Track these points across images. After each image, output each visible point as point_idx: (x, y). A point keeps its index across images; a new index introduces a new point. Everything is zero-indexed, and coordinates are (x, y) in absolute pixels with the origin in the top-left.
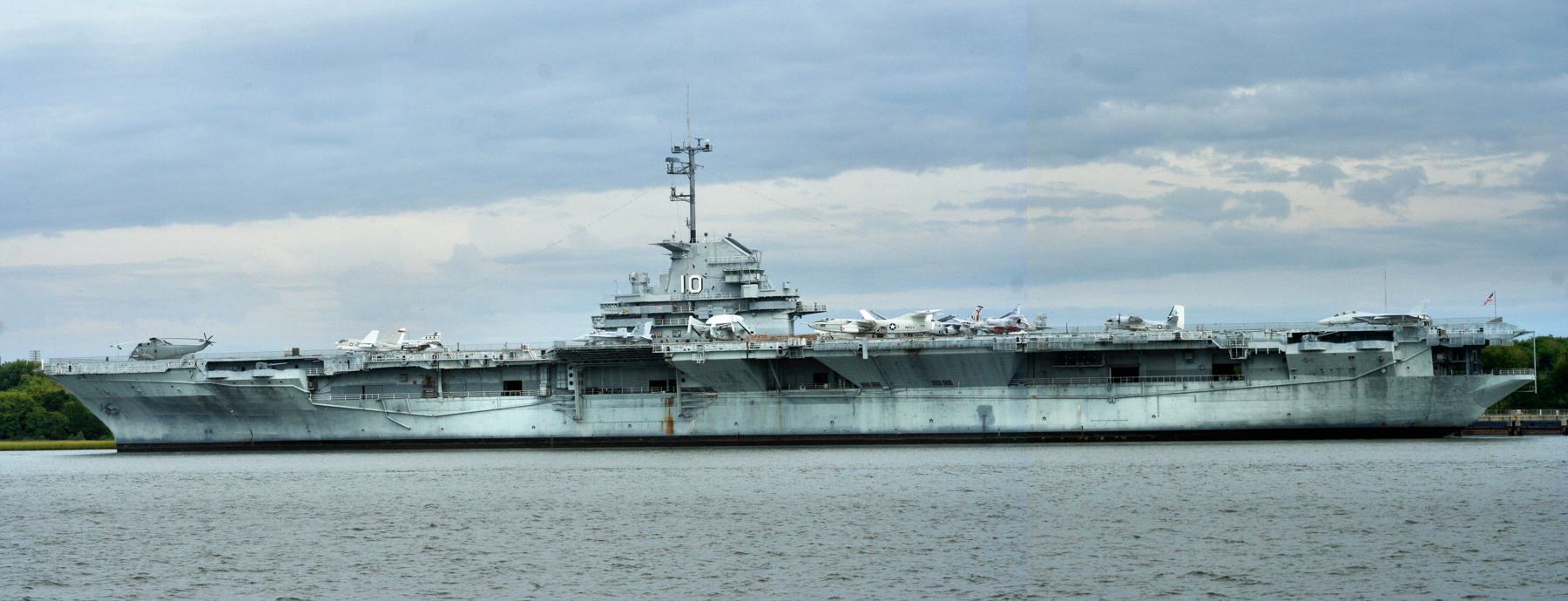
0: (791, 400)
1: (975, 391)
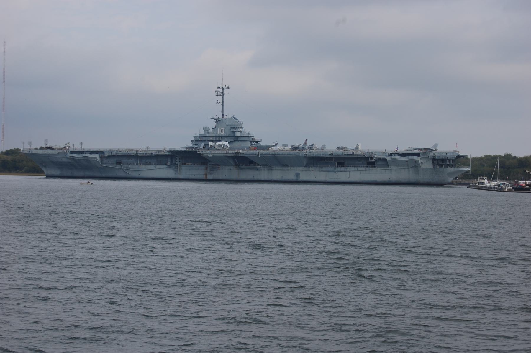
0: (242, 169)
1: (295, 168)
